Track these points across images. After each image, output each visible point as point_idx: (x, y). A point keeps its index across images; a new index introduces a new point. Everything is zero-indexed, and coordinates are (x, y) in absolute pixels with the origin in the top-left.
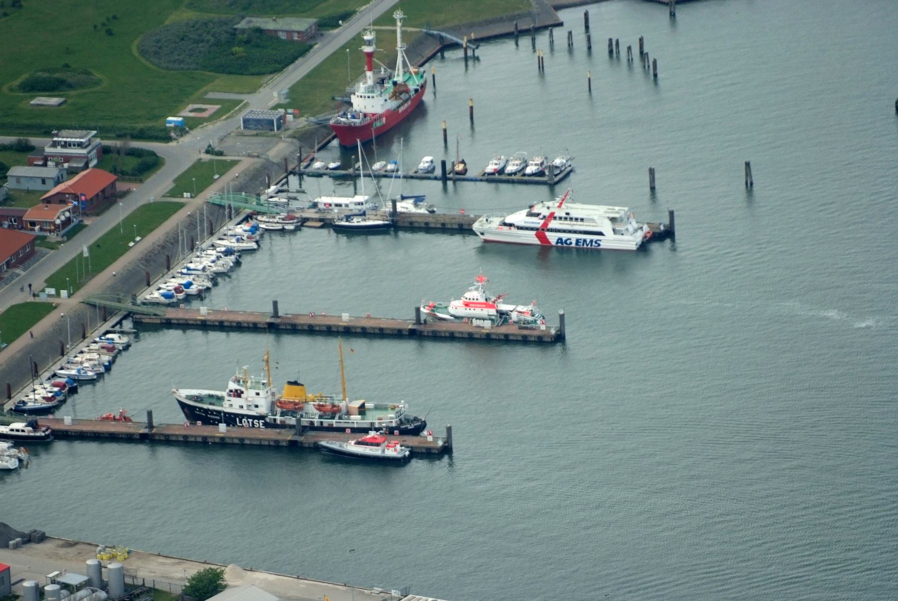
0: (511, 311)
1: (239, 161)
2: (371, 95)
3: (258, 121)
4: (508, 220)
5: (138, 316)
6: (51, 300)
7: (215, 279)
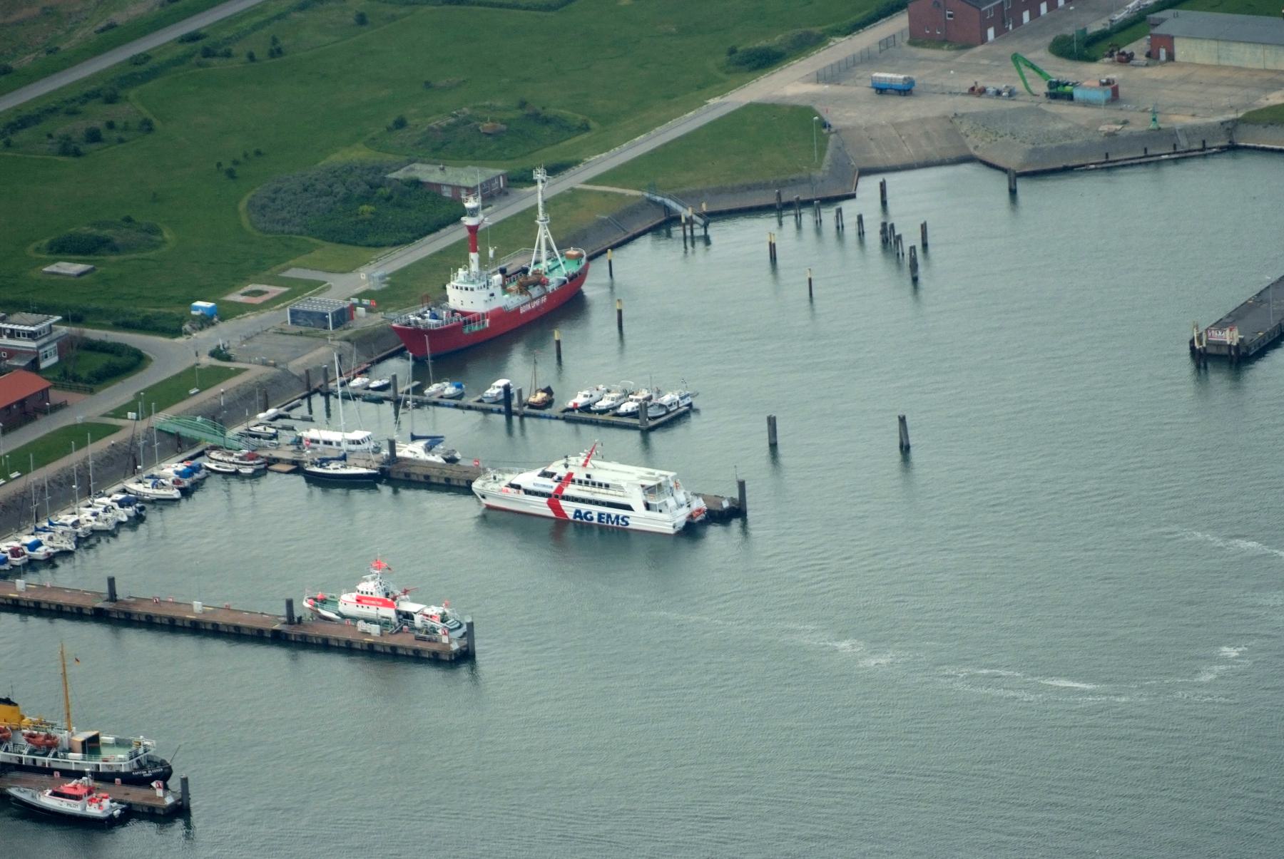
1: (246, 370)
2: (469, 286)
3: (309, 314)
7: (88, 539)
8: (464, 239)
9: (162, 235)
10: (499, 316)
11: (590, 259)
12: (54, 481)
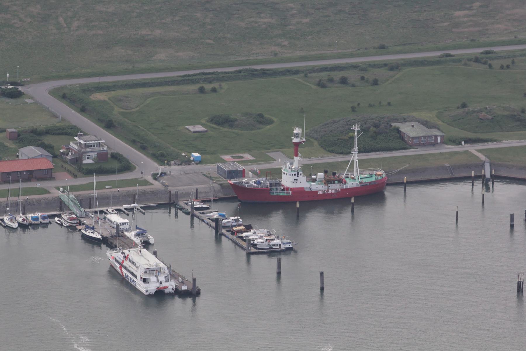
10: (299, 192)
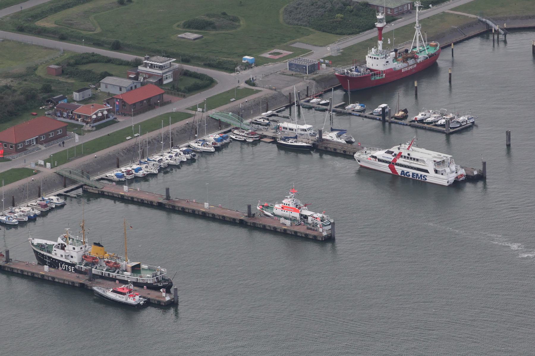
0: (309, 216)
3: (297, 66)
4: (374, 155)
5: (86, 187)
6: (37, 168)
7: (166, 169)
8: (376, 37)
9: (239, 22)
10: (390, 73)
11: (442, 48)
12: (155, 139)
